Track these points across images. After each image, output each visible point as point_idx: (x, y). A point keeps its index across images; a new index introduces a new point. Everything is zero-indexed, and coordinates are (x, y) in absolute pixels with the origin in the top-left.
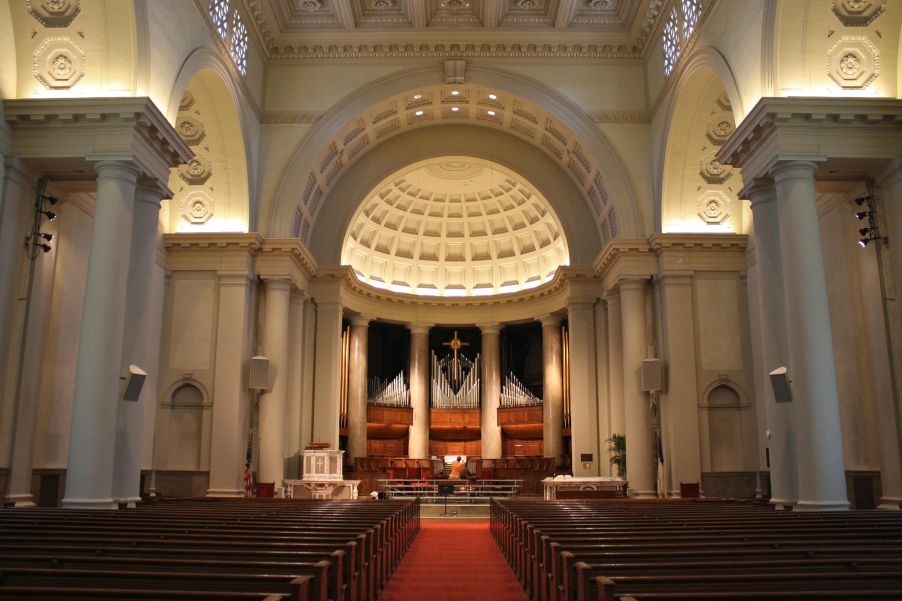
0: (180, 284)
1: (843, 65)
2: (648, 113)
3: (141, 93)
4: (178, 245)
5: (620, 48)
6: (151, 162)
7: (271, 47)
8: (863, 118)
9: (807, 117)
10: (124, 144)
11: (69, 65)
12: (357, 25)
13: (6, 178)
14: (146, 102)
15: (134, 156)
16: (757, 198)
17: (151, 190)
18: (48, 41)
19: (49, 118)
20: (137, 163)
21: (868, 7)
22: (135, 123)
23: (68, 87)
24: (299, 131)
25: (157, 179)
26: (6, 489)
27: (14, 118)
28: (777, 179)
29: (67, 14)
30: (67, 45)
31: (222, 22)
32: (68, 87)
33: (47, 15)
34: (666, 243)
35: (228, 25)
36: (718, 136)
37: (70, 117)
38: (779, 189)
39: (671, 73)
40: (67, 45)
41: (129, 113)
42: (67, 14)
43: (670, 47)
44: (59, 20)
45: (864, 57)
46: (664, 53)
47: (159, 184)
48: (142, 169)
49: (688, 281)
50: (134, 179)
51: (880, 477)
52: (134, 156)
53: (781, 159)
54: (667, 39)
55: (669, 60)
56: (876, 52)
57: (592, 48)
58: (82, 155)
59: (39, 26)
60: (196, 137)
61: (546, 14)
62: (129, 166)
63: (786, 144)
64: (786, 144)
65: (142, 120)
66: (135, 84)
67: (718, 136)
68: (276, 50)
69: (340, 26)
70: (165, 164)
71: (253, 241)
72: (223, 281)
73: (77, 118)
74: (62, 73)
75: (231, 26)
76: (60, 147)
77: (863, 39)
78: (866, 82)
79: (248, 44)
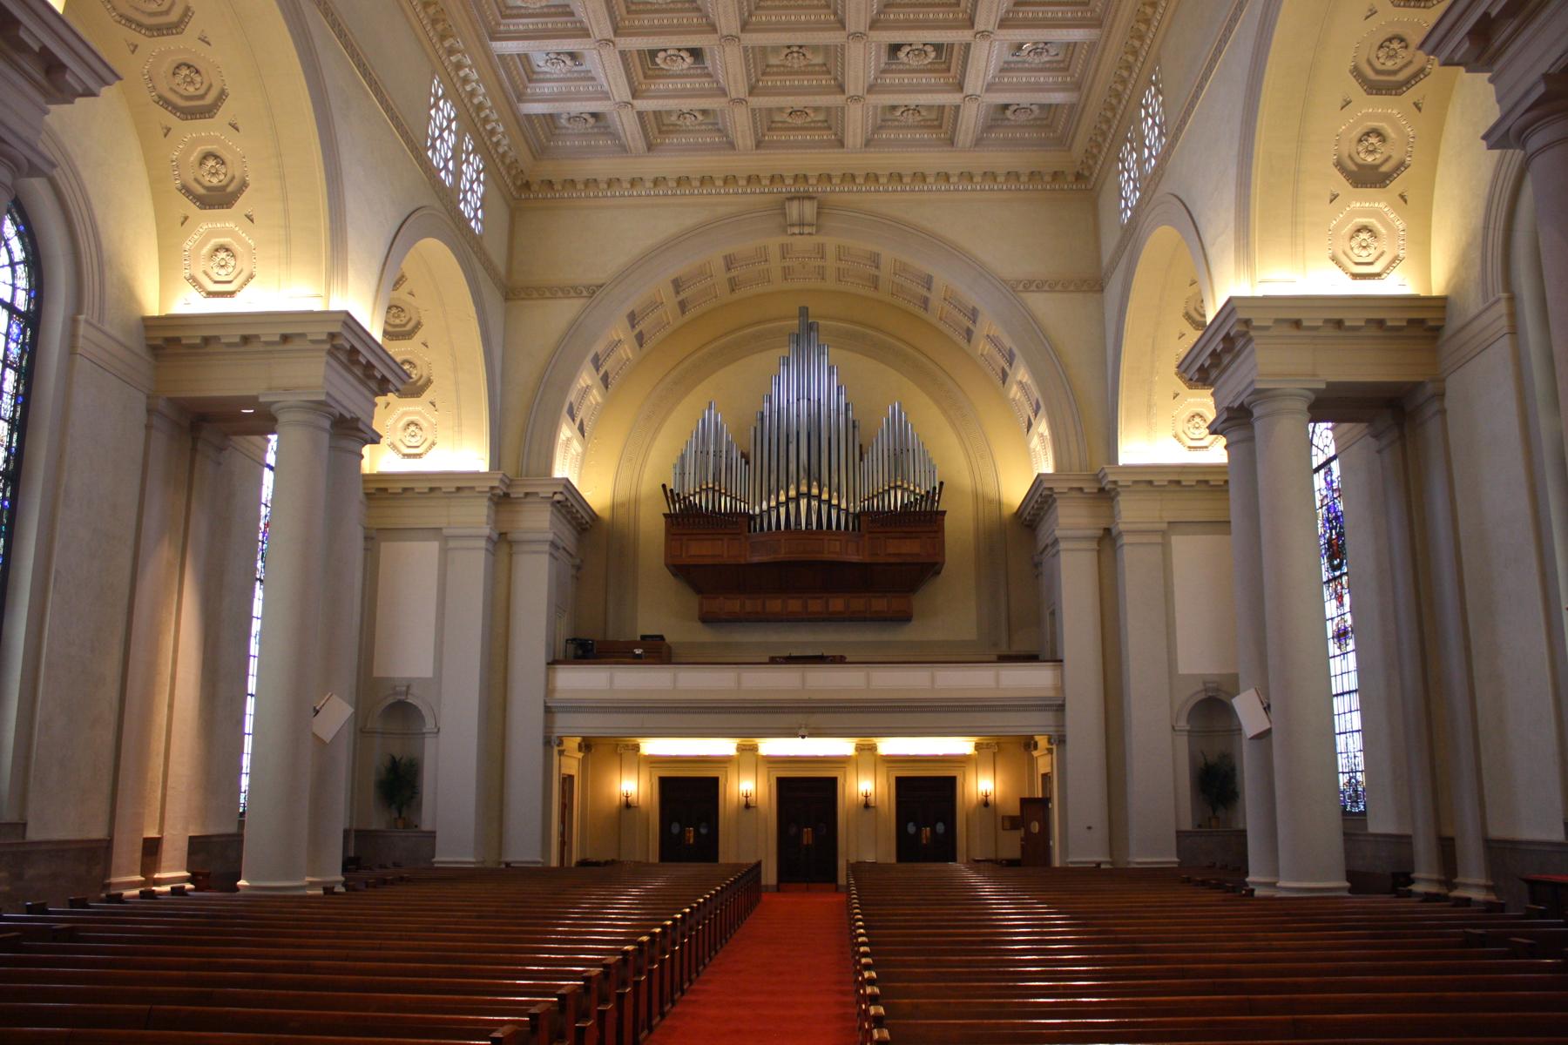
0: (387, 548)
1: (1354, 243)
2: (1097, 280)
3: (337, 303)
4: (383, 490)
5: (1056, 175)
6: (348, 394)
7: (519, 183)
8: (1380, 323)
9: (1297, 324)
10: (311, 375)
11: (232, 262)
12: (650, 147)
13: (148, 427)
14: (343, 317)
15: (328, 394)
16: (1235, 436)
17: (352, 431)
18: (205, 227)
19: (207, 340)
20: (332, 403)
21: (1387, 160)
22: (328, 346)
23: (231, 294)
24: (563, 312)
25: (358, 419)
26: (107, 872)
27: (159, 342)
28: (1257, 412)
29: (230, 189)
30: (230, 233)
31: (446, 161)
32: (231, 294)
33: (201, 191)
34: (1123, 480)
35: (455, 165)
36: (1378, 72)
37: (237, 340)
38: (1258, 426)
39: (1130, 220)
40: (230, 233)
41: (320, 332)
42: (230, 189)
43: (1152, 128)
44: (218, 199)
45: (1383, 231)
46: (1120, 189)
47: (361, 426)
48: (338, 410)
49: (1158, 539)
50: (327, 424)
51: (1410, 844)
52: (328, 394)
53: (1259, 386)
54: (1147, 113)
55: (1150, 148)
56: (1400, 224)
57: (1012, 175)
58: (254, 393)
59: (192, 209)
60: (408, 327)
61: (940, 126)
62: (319, 407)
63: (1267, 363)
64: (1267, 363)
65: (338, 342)
66: (328, 286)
67: (1378, 72)
68: (527, 185)
69: (624, 149)
70: (367, 393)
71: (496, 484)
72: (452, 544)
73: (246, 339)
74: (223, 272)
75: (458, 165)
76: (224, 382)
77: (1381, 205)
78: (1387, 268)
79: (484, 183)
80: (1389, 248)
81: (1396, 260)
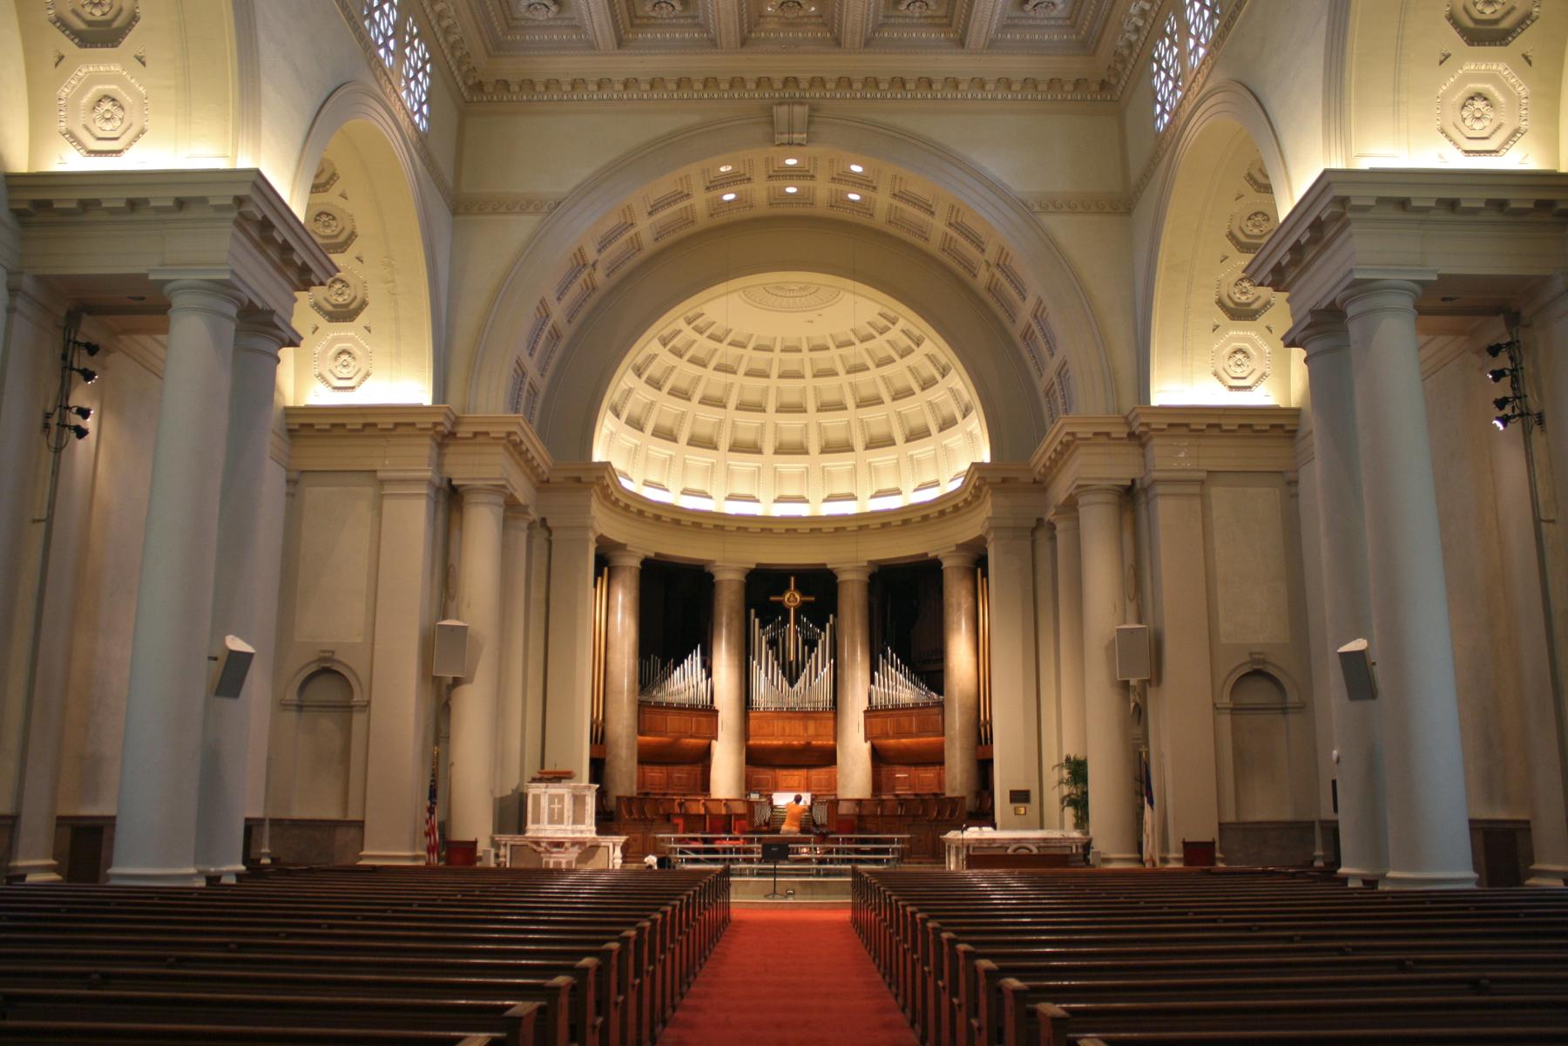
0: (314, 493)
1: (1465, 114)
3: (244, 162)
4: (309, 427)
5: (1077, 84)
6: (262, 282)
7: (470, 82)
8: (1500, 205)
9: (1403, 204)
10: (215, 250)
11: (120, 114)
12: (620, 43)
13: (11, 310)
14: (253, 177)
15: (233, 272)
16: (1317, 345)
17: (262, 331)
18: (83, 71)
19: (85, 205)
20: (238, 284)
21: (1508, 13)
22: (234, 215)
23: (118, 152)
24: (520, 228)
25: (272, 312)
27: (25, 206)
28: (1351, 311)
29: (116, 24)
30: (116, 79)
31: (387, 38)
32: (118, 152)
33: (81, 26)
34: (1157, 423)
38: (1354, 329)
39: (1167, 127)
40: (116, 79)
41: (224, 197)
42: (116, 24)
44: (102, 35)
45: (1501, 99)
46: (1155, 93)
47: (276, 320)
48: (247, 294)
49: (1196, 489)
50: (233, 311)
51: (1529, 830)
52: (233, 272)
53: (1358, 276)
56: (1522, 90)
57: (1030, 83)
58: (143, 271)
59: (68, 46)
60: (341, 239)
61: (950, 25)
62: (224, 289)
63: (1366, 251)
64: (1366, 251)
65: (246, 208)
66: (235, 147)
68: (479, 86)
69: (591, 46)
70: (287, 286)
71: (440, 419)
72: (388, 490)
73: (133, 205)
74: (108, 126)
75: (401, 45)
76: (105, 257)
77: (1499, 68)
78: (1506, 142)
79: (431, 76)
80: (1257, 365)
81: (1263, 375)
